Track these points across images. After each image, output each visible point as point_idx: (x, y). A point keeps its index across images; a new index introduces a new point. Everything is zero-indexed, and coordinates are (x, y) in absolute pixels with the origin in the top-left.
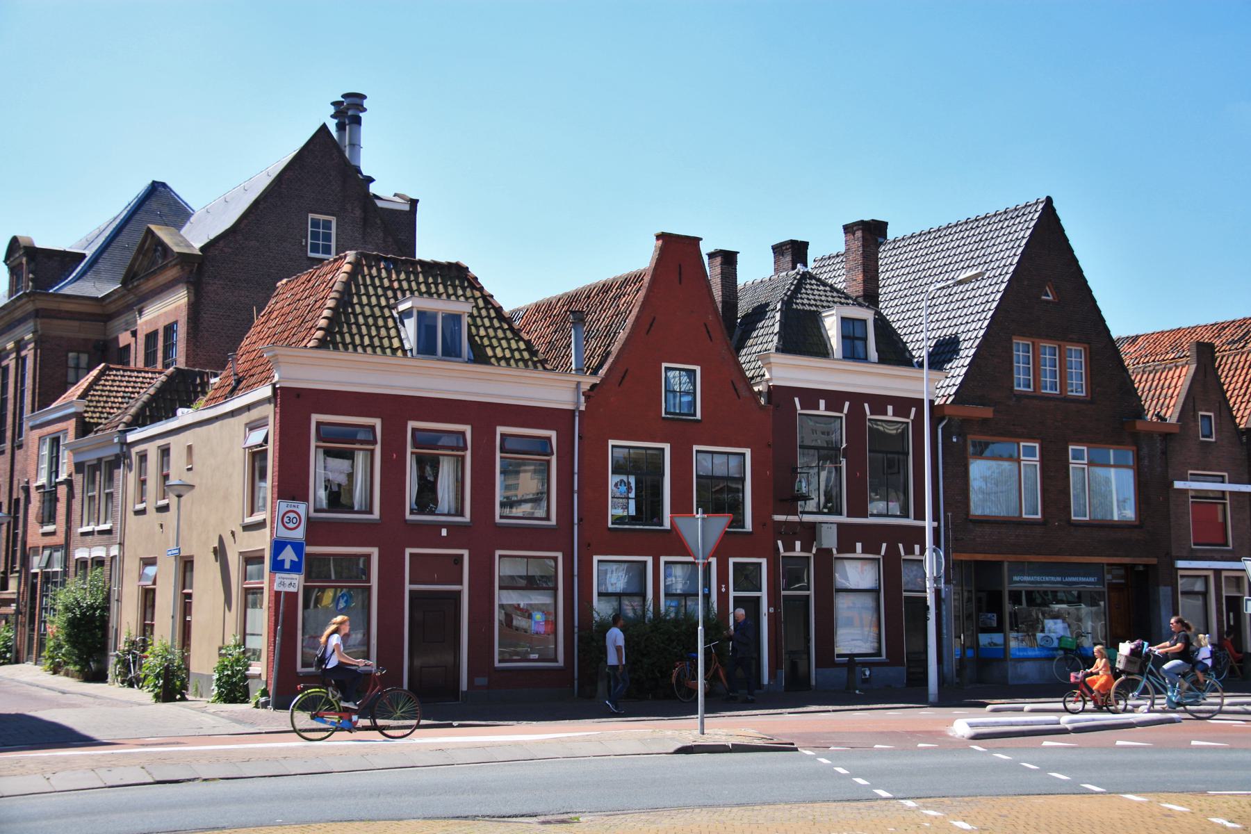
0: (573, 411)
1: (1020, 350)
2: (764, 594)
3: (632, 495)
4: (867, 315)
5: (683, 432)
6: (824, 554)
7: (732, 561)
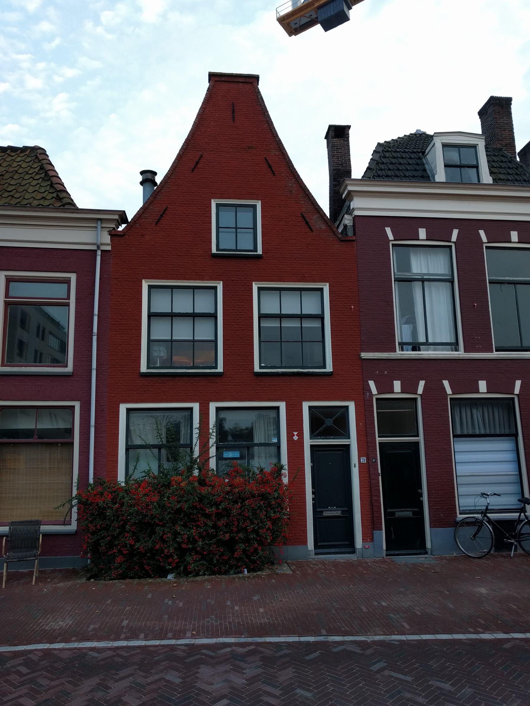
2: (353, 442)
5: (237, 270)
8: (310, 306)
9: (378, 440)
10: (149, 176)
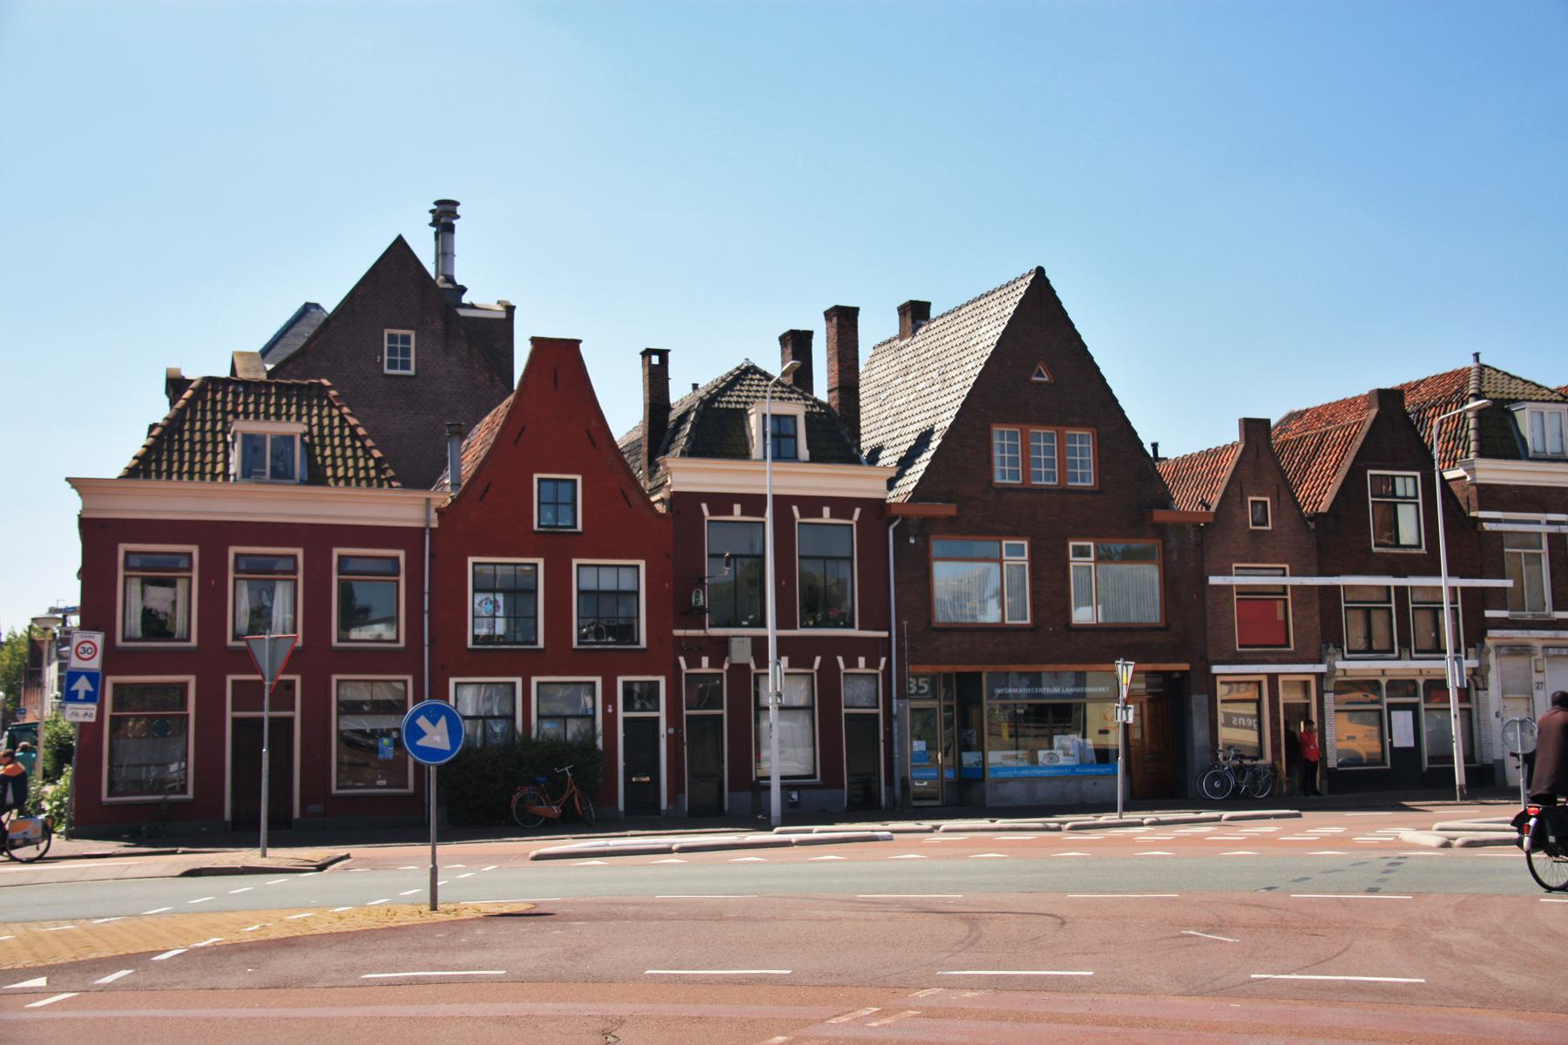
0: (423, 529)
1: (1003, 441)
2: (662, 714)
3: (501, 613)
4: (798, 409)
5: (559, 548)
6: (740, 670)
7: (620, 680)
8: (626, 583)
9: (685, 712)
10: (450, 208)
